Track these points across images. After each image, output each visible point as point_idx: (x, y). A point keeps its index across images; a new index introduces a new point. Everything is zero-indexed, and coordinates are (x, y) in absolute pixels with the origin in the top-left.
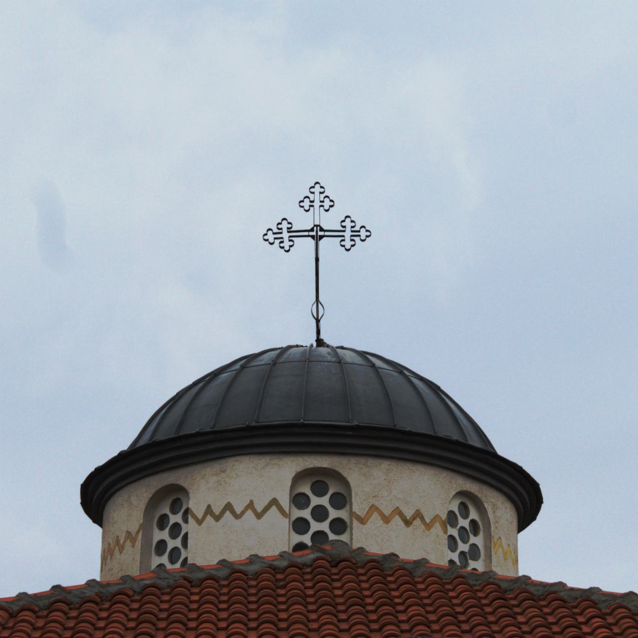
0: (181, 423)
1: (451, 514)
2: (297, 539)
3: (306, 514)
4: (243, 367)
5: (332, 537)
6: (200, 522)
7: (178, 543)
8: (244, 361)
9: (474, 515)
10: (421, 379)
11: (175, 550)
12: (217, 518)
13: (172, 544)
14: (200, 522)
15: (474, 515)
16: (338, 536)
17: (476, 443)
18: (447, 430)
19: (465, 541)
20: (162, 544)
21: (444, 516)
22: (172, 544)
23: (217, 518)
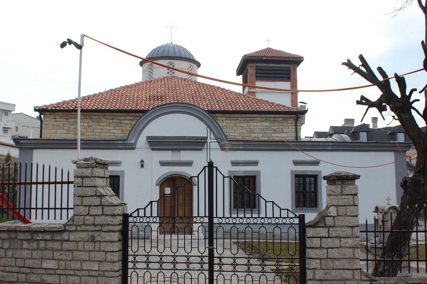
0: (152, 55)
1: (188, 68)
2: (168, 75)
3: (169, 71)
4: (161, 47)
5: (172, 74)
6: (155, 69)
7: (152, 71)
8: (159, 228)
9: (191, 68)
10: (185, 49)
11: (152, 72)
12: (157, 68)
13: (151, 71)
14: (155, 69)
15: (191, 68)
16: (176, 153)
17: (192, 58)
18: (188, 57)
19: (190, 78)
20: (150, 72)
21: (187, 68)
22: (151, 71)
23: (157, 68)
